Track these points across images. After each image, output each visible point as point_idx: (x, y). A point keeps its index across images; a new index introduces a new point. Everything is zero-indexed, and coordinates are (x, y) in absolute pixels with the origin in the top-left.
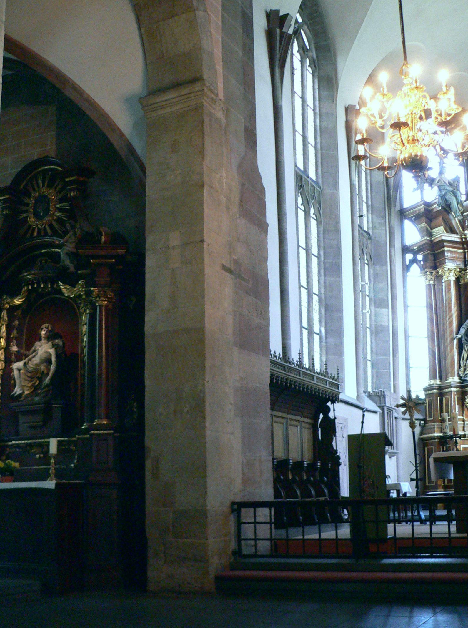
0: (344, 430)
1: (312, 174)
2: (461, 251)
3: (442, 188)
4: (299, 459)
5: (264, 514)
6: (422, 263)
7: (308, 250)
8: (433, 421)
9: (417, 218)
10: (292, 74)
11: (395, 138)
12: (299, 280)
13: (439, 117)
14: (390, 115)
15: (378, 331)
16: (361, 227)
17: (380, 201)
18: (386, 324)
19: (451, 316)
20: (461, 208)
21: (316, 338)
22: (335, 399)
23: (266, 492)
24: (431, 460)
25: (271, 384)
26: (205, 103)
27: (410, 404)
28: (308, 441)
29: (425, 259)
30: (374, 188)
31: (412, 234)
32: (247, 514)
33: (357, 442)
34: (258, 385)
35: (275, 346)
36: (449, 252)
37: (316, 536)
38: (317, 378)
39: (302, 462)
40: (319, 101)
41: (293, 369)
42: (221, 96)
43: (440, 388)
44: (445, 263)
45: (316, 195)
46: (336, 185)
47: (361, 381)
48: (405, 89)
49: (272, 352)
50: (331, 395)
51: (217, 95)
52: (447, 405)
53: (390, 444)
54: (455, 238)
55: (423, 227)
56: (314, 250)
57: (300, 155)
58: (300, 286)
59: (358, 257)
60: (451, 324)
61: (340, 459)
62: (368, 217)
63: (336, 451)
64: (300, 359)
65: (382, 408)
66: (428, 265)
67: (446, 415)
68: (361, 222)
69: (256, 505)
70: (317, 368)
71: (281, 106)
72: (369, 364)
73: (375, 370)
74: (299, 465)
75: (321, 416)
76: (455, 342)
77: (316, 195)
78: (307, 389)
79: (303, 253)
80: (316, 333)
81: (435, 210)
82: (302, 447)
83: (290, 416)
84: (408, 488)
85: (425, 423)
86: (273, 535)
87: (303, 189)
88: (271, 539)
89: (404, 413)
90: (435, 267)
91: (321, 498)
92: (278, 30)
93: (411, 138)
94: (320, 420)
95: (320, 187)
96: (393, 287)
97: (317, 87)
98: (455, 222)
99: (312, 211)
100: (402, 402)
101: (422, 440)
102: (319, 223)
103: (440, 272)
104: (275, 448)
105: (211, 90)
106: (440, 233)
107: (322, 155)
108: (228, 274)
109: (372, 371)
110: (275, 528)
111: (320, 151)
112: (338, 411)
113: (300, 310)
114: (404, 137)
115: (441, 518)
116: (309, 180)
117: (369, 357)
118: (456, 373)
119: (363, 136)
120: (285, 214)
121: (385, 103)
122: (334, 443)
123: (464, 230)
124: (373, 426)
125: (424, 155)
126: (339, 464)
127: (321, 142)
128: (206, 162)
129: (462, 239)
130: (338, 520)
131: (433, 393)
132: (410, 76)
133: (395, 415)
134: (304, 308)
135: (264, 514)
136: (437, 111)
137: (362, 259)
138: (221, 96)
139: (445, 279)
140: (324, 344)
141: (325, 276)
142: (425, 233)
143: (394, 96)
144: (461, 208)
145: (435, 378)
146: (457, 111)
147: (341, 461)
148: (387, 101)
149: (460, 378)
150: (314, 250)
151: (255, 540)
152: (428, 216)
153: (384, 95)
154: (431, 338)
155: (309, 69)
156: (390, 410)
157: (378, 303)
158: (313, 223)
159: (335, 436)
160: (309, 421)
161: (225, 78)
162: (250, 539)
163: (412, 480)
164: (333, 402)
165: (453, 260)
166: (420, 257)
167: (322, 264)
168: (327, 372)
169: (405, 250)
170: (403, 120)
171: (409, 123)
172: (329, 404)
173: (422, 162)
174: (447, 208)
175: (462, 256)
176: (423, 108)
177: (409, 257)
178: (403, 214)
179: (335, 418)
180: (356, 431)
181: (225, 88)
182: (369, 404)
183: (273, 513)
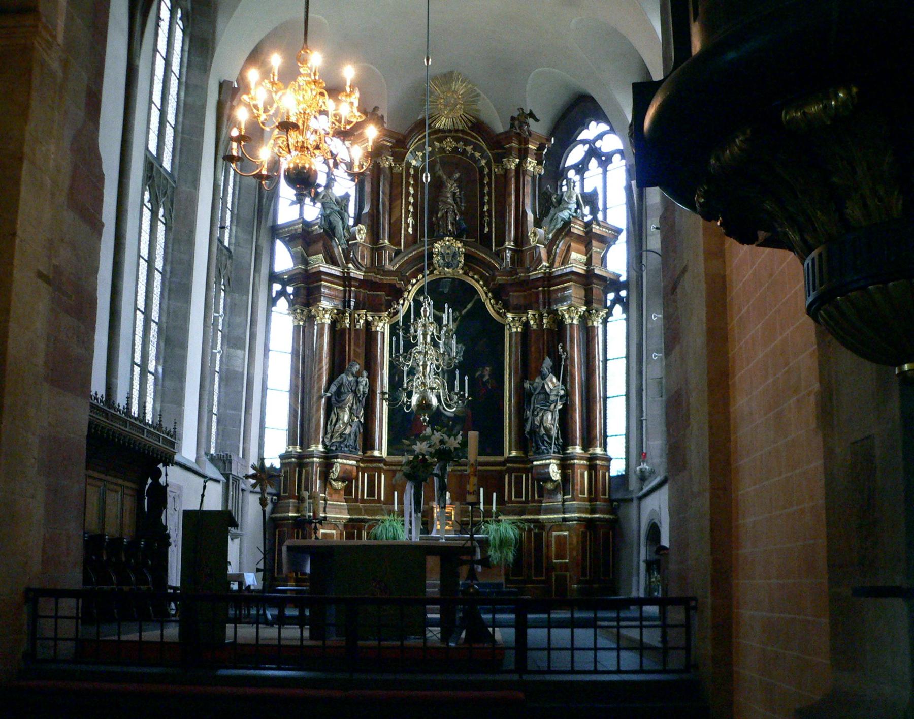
0: (178, 501)
1: (167, 164)
2: (341, 288)
3: (327, 205)
4: (117, 535)
5: (68, 606)
6: (292, 297)
7: (150, 262)
8: (289, 498)
10: (158, 26)
11: (280, 142)
12: (136, 300)
13: (337, 124)
14: (278, 109)
15: (229, 378)
16: (221, 241)
17: (248, 212)
18: (240, 370)
19: (321, 369)
20: (346, 234)
21: (151, 378)
22: (169, 460)
23: (73, 578)
24: (284, 549)
25: (89, 437)
26: (36, 44)
27: (263, 475)
29: (296, 293)
30: (243, 191)
31: (284, 259)
32: (46, 606)
33: (196, 521)
34: (72, 436)
35: (98, 386)
36: (326, 287)
37: (134, 637)
38: (149, 432)
39: (121, 539)
40: (188, 68)
41: (119, 418)
42: (60, 39)
43: (300, 457)
44: (320, 301)
45: (169, 193)
46: (195, 183)
47: (203, 440)
48: (301, 80)
49: (93, 393)
50: (141, 446)
51: (55, 37)
52: (307, 479)
53: (235, 525)
54: (335, 271)
55: (297, 252)
56: (159, 264)
57: (155, 136)
58: (136, 309)
61: (169, 537)
62: (231, 230)
63: (166, 527)
64: (128, 404)
65: (226, 476)
66: (299, 300)
67: (306, 494)
68: (222, 234)
69: (58, 594)
70: (149, 417)
71: (138, 66)
72: (214, 418)
73: (221, 427)
74: (116, 542)
75: (150, 481)
76: (323, 401)
77: (171, 193)
78: (134, 445)
79: (143, 265)
80: (151, 373)
81: (315, 233)
82: (122, 521)
83: (109, 478)
84: (251, 579)
85: (279, 499)
86: (80, 634)
87: (153, 181)
88: (76, 639)
89: (254, 486)
91: (124, 588)
93: (299, 145)
94: (147, 487)
95: (175, 182)
97: (186, 48)
98: (338, 251)
100: (252, 471)
101: (273, 520)
104: (87, 519)
105: (46, 27)
106: (319, 263)
107: (182, 139)
108: (45, 285)
109: (217, 429)
110: (82, 624)
111: (180, 135)
112: (172, 476)
113: (134, 340)
114: (292, 141)
115: (292, 621)
116: (162, 170)
117: (215, 410)
118: (321, 439)
119: (240, 132)
121: (274, 95)
122: (163, 518)
123: (347, 263)
124: (214, 501)
125: (313, 167)
126: (169, 544)
127: (183, 123)
128: (30, 127)
129: (343, 273)
130: (163, 618)
131: (291, 463)
132: (309, 65)
133: (242, 486)
134: (138, 336)
135: (68, 606)
136: (335, 115)
137: (218, 283)
138: (60, 39)
139: (318, 320)
140: (160, 388)
141: (169, 299)
142: (299, 260)
143: (286, 87)
144: (346, 234)
145: (294, 444)
146: (359, 120)
147: (171, 540)
148: (276, 92)
149: (325, 446)
150: (159, 264)
151: (56, 639)
152: (304, 238)
153: (273, 83)
154: (293, 392)
155: (180, 23)
156: (236, 479)
157: (233, 341)
158: (161, 228)
159: (165, 507)
160: (133, 486)
161: (70, 18)
162: (46, 639)
163: (258, 570)
164: (166, 465)
165: (330, 298)
166: (290, 289)
167: (167, 283)
168: (160, 425)
169: (273, 277)
170: (293, 119)
171: (300, 124)
172: (160, 466)
173: (309, 176)
174: (330, 231)
175: (341, 295)
176: (318, 108)
177: (277, 287)
178: (275, 232)
179: (167, 485)
180: (193, 505)
181: (67, 29)
182: (211, 470)
183: (80, 604)
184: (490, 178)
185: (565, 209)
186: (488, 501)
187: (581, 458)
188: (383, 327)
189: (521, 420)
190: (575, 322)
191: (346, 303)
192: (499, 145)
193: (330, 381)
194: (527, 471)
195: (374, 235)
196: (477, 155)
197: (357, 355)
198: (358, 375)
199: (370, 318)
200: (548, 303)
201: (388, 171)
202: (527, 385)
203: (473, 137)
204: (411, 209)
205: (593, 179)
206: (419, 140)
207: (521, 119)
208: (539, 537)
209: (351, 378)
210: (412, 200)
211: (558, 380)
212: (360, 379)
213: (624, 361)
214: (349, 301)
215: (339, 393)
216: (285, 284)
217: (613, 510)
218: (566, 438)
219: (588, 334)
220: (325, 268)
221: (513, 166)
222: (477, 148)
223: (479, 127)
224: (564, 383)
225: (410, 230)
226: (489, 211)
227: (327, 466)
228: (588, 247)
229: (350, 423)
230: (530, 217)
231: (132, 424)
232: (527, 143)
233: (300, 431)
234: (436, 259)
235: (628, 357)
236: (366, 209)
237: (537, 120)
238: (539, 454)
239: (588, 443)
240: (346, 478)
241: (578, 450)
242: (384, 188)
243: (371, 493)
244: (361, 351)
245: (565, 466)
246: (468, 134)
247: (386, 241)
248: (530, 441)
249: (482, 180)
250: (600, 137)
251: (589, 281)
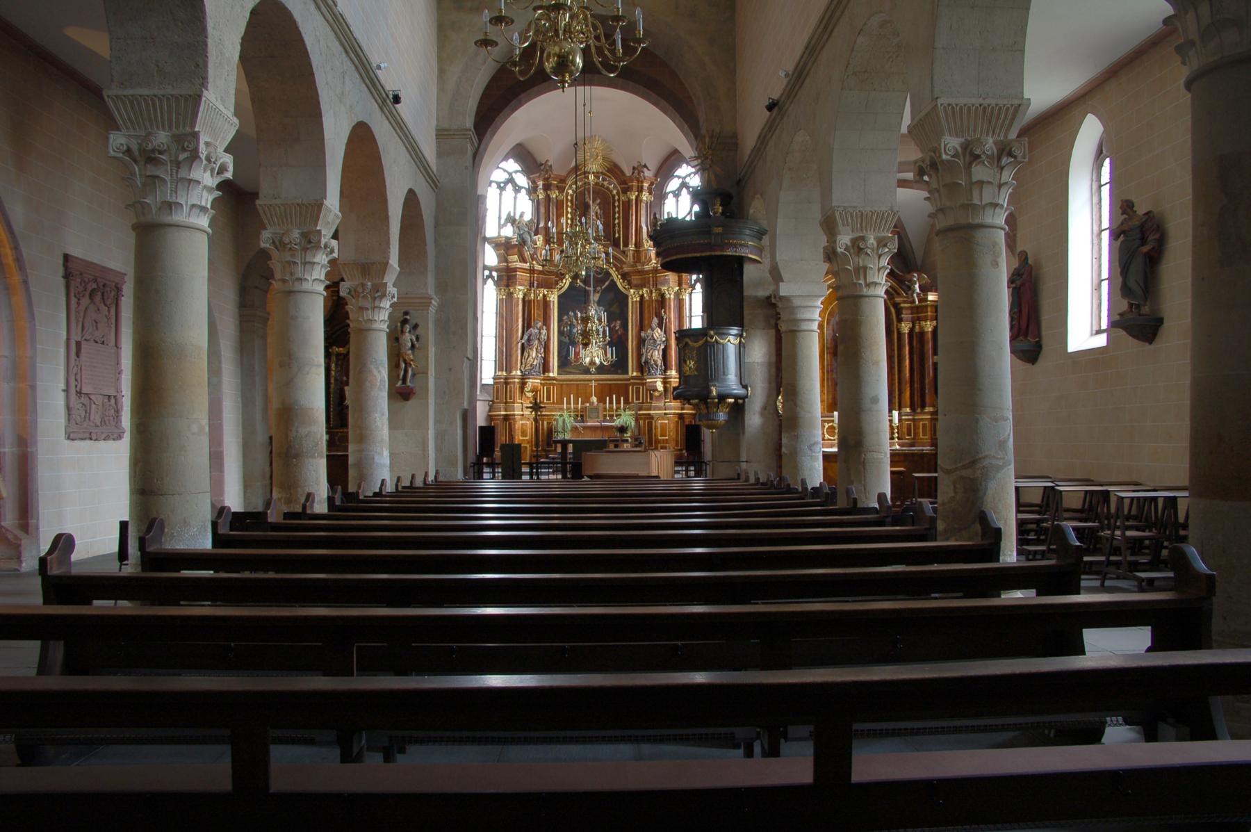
31: (490, 257)
54: (527, 266)
169: (485, 268)
177: (487, 273)
186: (618, 402)
188: (554, 298)
189: (639, 355)
191: (531, 285)
194: (643, 384)
200: (656, 283)
202: (643, 334)
207: (639, 168)
208: (650, 424)
215: (529, 340)
218: (666, 366)
219: (680, 303)
220: (519, 265)
227: (523, 384)
229: (536, 358)
233: (505, 361)
240: (534, 390)
242: (553, 210)
243: (548, 398)
244: (541, 313)
245: (665, 383)
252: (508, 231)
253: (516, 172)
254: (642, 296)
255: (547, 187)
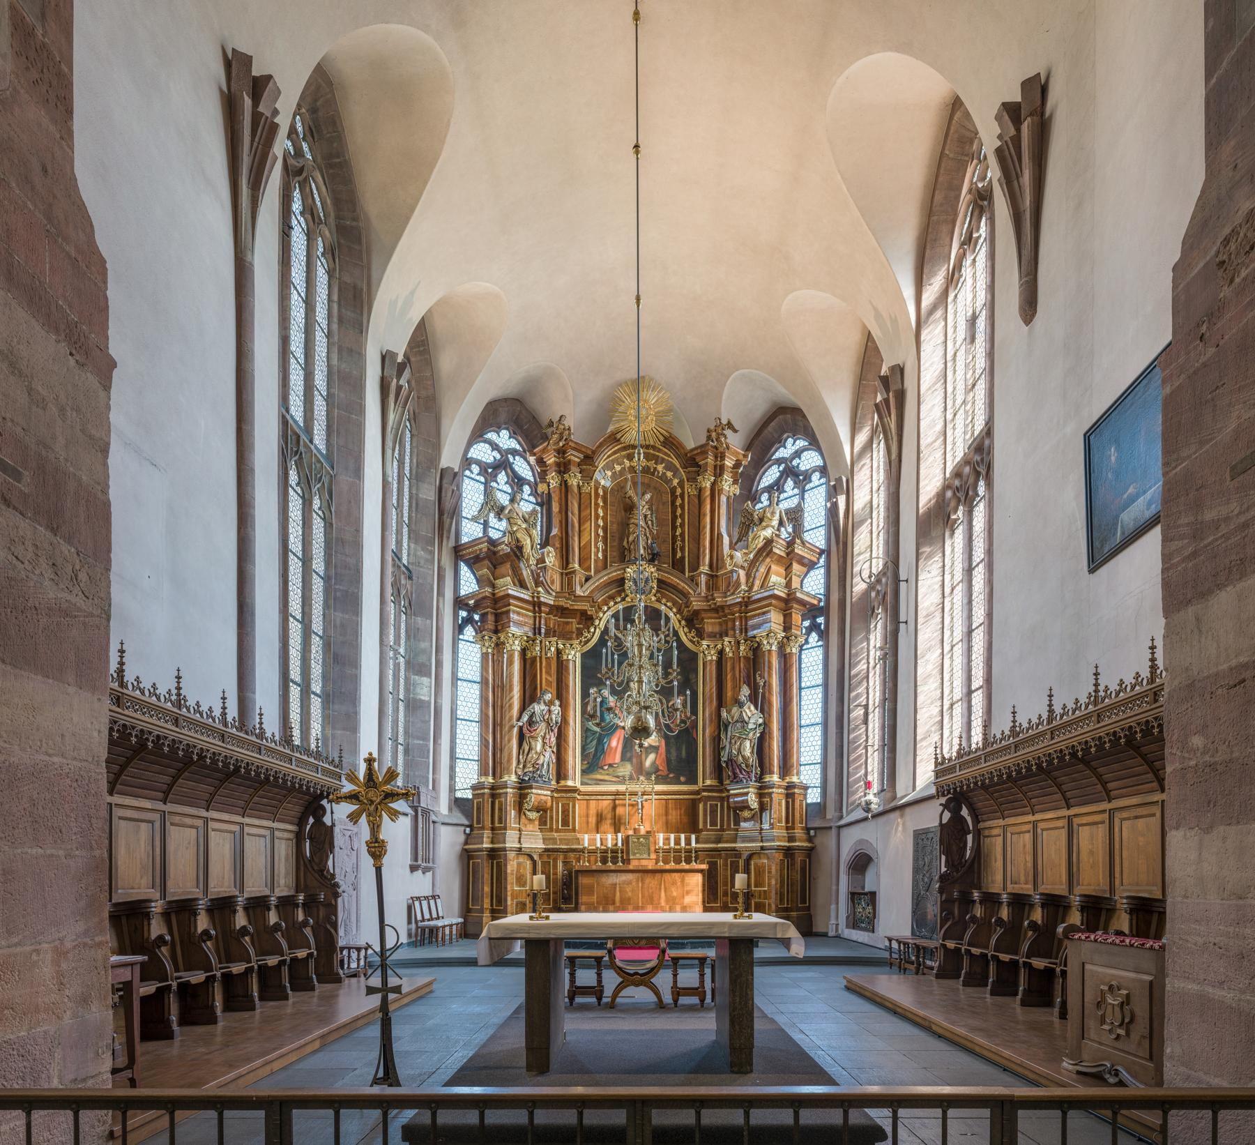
7: (306, 561)
9: (474, 563)
18: (427, 699)
28: (287, 859)
52: (500, 809)
54: (525, 595)
59: (389, 597)
60: (511, 707)
63: (333, 876)
65: (415, 809)
74: (257, 905)
75: (311, 820)
76: (516, 730)
87: (301, 457)
90: (496, 631)
92: (248, 102)
96: (439, 650)
97: (335, 298)
98: (526, 573)
99: (316, 503)
102: (328, 526)
103: (502, 639)
106: (507, 585)
120: (253, 470)
122: (330, 863)
145: (486, 774)
169: (459, 603)
175: (531, 622)
179: (333, 825)
184: (683, 499)
185: (767, 526)
187: (780, 787)
188: (574, 656)
190: (774, 648)
191: (536, 630)
192: (692, 462)
193: (523, 709)
195: (565, 559)
196: (669, 474)
197: (549, 683)
198: (550, 703)
199: (561, 646)
201: (576, 490)
202: (724, 714)
203: (666, 454)
204: (601, 532)
205: (789, 500)
206: (615, 453)
207: (718, 430)
209: (543, 707)
210: (601, 523)
211: (756, 708)
212: (553, 708)
213: (819, 690)
214: (540, 629)
215: (531, 722)
216: (471, 610)
217: (810, 839)
219: (785, 658)
221: (708, 485)
222: (670, 467)
223: (670, 442)
224: (762, 711)
225: (600, 555)
226: (682, 534)
227: (521, 798)
228: (788, 568)
230: (726, 540)
231: (269, 750)
232: (723, 457)
233: (492, 760)
234: (628, 584)
235: (826, 685)
236: (555, 531)
237: (735, 431)
238: (735, 779)
239: (786, 769)
241: (775, 778)
244: (553, 679)
246: (659, 451)
247: (577, 566)
248: (724, 770)
249: (673, 502)
250: (798, 454)
251: (788, 603)
252: (498, 528)
253: (514, 452)
254: (721, 653)
255: (563, 468)
